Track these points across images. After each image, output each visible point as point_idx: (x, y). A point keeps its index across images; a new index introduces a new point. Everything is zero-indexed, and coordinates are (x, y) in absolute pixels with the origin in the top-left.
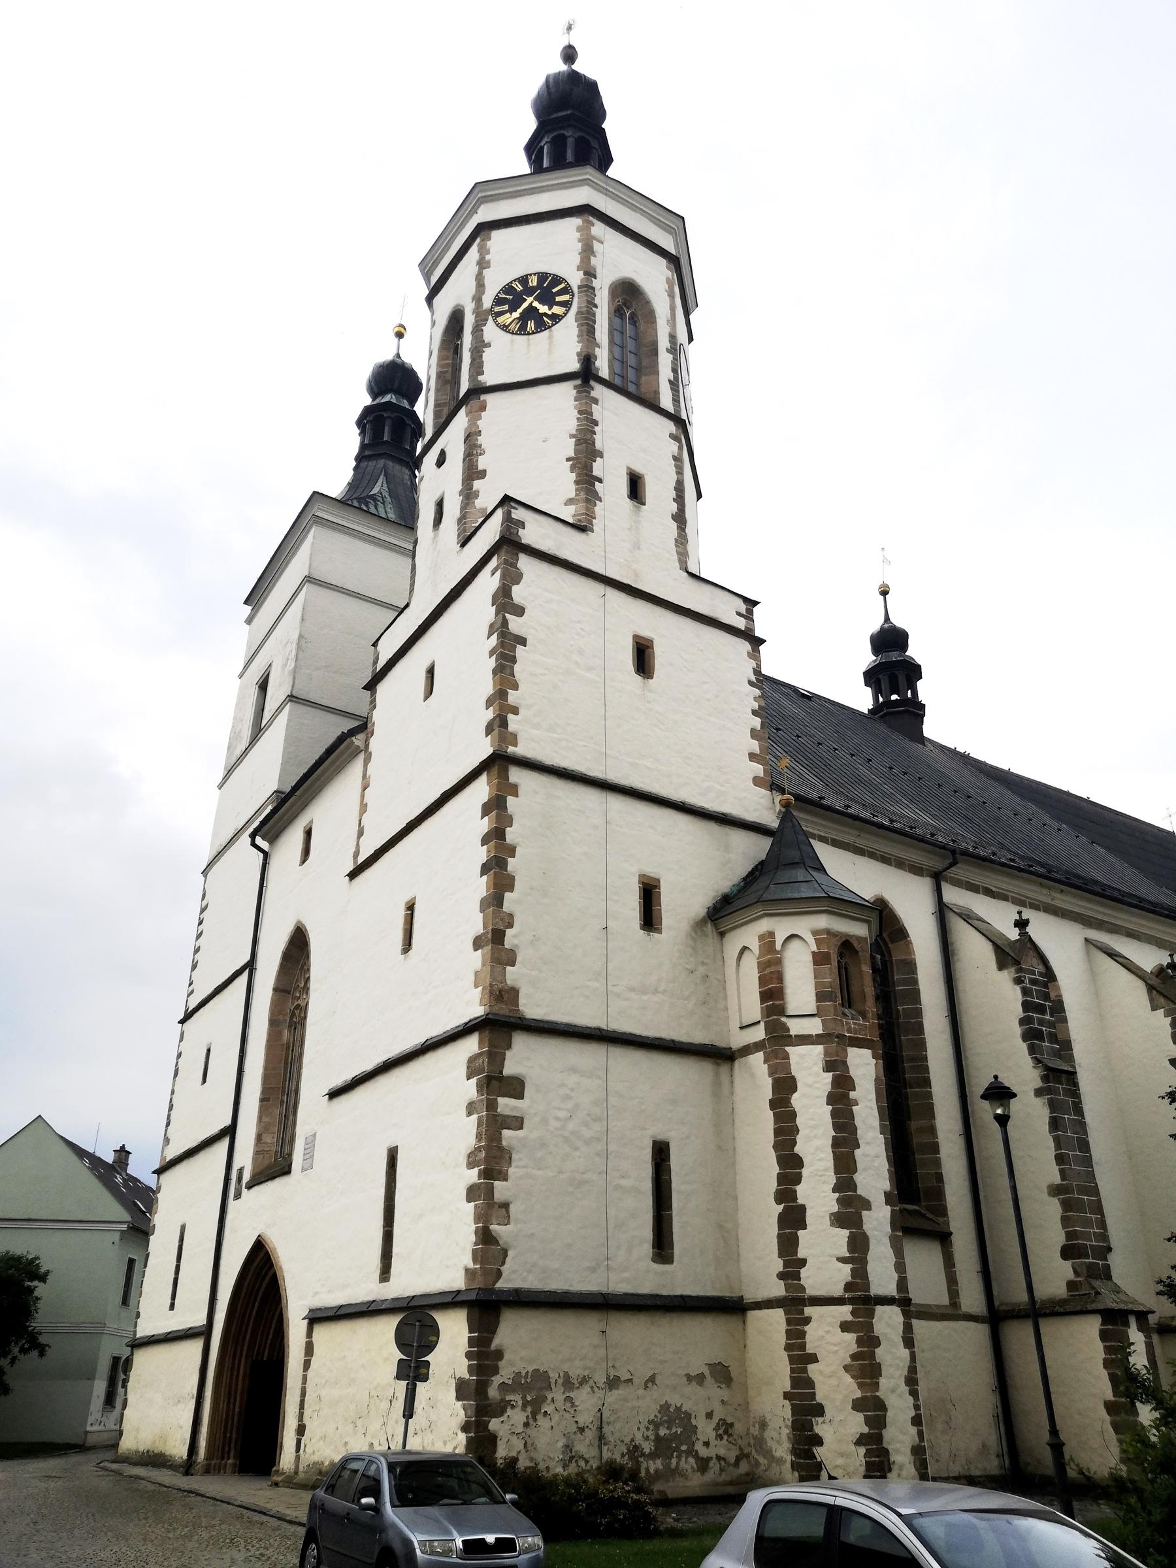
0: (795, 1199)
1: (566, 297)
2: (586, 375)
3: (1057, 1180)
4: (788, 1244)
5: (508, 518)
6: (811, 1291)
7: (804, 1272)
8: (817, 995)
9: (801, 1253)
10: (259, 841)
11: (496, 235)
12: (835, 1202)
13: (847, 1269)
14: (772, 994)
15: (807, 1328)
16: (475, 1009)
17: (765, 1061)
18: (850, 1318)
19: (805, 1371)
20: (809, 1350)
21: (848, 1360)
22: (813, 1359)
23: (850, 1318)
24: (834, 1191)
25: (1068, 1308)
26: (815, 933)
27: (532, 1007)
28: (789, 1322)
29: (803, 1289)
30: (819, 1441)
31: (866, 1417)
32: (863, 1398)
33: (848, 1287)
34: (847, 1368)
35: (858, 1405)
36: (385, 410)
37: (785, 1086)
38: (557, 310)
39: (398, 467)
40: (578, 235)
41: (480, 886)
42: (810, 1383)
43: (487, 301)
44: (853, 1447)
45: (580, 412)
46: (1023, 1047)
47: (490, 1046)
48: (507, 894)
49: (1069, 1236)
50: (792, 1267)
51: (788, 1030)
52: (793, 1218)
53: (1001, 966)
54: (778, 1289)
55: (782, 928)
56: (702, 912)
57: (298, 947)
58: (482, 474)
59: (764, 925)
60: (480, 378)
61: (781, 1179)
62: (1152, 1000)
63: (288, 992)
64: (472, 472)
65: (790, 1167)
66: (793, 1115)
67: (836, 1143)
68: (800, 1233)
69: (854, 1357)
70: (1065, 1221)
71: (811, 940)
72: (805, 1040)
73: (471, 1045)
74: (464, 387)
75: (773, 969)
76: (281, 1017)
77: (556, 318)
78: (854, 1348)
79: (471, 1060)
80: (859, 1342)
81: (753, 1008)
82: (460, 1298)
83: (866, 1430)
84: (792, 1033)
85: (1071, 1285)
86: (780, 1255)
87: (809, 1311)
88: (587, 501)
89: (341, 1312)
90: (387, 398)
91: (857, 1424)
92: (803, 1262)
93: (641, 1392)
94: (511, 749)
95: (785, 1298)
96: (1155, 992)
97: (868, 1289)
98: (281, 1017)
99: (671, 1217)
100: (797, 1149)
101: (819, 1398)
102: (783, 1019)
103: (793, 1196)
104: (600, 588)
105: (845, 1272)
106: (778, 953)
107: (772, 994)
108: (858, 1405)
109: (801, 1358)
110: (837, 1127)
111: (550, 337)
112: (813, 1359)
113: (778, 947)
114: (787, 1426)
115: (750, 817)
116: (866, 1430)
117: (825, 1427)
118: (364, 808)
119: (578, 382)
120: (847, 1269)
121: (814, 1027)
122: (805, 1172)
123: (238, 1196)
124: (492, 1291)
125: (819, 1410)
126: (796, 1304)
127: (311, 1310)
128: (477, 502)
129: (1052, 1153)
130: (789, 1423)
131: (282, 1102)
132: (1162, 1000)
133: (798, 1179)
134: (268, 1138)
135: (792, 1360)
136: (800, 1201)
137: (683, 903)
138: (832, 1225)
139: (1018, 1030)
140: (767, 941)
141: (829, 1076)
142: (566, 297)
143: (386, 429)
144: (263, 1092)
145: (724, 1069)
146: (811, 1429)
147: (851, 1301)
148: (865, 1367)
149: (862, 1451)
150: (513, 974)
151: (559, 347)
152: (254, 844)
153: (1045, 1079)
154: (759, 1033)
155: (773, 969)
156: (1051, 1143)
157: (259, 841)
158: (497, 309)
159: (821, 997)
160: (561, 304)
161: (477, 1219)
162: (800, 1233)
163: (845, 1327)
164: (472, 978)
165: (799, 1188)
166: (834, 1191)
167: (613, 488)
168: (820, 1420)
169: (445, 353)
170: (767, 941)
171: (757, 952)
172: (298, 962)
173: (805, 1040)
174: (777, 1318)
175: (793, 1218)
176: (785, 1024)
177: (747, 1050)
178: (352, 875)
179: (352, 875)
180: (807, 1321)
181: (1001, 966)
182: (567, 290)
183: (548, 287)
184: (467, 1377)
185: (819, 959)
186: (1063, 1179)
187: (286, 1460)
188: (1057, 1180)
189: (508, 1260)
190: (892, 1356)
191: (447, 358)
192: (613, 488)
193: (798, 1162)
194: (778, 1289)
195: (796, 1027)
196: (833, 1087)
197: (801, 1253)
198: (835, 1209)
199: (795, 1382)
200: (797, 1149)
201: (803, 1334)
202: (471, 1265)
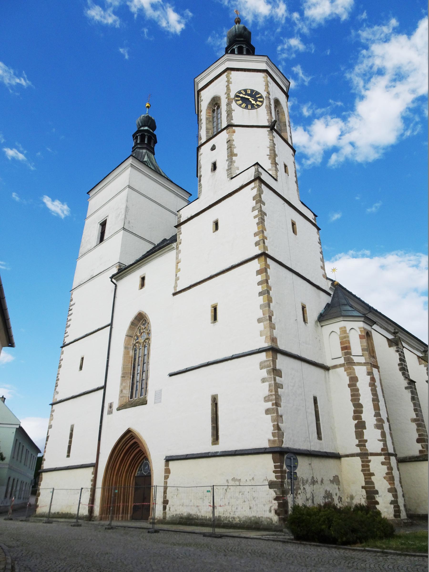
0: (361, 419)
1: (262, 100)
2: (272, 127)
3: (415, 417)
4: (359, 435)
5: (257, 171)
6: (370, 451)
7: (367, 444)
8: (362, 349)
9: (365, 438)
10: (113, 280)
11: (233, 72)
12: (375, 420)
13: (382, 443)
14: (346, 348)
15: (370, 464)
16: (265, 345)
17: (345, 371)
18: (384, 460)
19: (370, 479)
20: (371, 471)
21: (385, 475)
22: (373, 474)
23: (384, 460)
24: (374, 416)
25: (421, 459)
26: (360, 328)
27: (281, 346)
28: (362, 462)
29: (367, 450)
30: (377, 503)
31: (393, 495)
32: (391, 488)
33: (382, 450)
34: (384, 478)
35: (390, 491)
36: (146, 132)
37: (353, 380)
38: (258, 103)
39: (150, 153)
40: (263, 79)
41: (261, 300)
42: (372, 483)
43: (232, 95)
44: (389, 505)
45: (270, 140)
46: (400, 373)
47: (273, 357)
48: (271, 304)
49: (420, 435)
50: (362, 443)
51: (353, 360)
52: (360, 426)
53: (390, 346)
54: (358, 450)
55: (349, 325)
56: (317, 319)
57: (141, 319)
58: (236, 155)
59: (342, 324)
60: (232, 121)
61: (355, 412)
62: (419, 362)
63: (132, 337)
64: (231, 154)
65: (358, 409)
66: (358, 390)
67: (373, 400)
68: (364, 431)
69: (387, 474)
70: (418, 430)
71: (358, 330)
72: (359, 364)
73: (263, 356)
74: (224, 125)
75: (346, 339)
76: (129, 346)
77: (259, 106)
78: (386, 471)
79: (261, 363)
80: (388, 468)
81: (339, 352)
82: (267, 450)
83: (393, 499)
84: (355, 361)
85: (420, 451)
86: (357, 438)
87: (370, 458)
88: (276, 170)
89: (188, 457)
90: (146, 128)
91: (390, 497)
92: (366, 441)
93: (320, 486)
94: (267, 252)
95: (361, 453)
96: (420, 359)
97: (388, 451)
98: (129, 346)
99: (320, 423)
100: (360, 402)
101: (376, 488)
102: (352, 357)
103: (360, 418)
104: (283, 202)
105: (381, 445)
106: (348, 334)
107: (346, 348)
108: (390, 491)
109: (368, 474)
110: (373, 394)
111: (257, 112)
112: (373, 474)
113: (348, 332)
114: (364, 498)
115: (324, 288)
116: (393, 499)
117: (379, 498)
118: (178, 270)
119: (269, 129)
120: (382, 443)
121: (362, 360)
122: (364, 409)
123: (110, 412)
124: (281, 448)
125: (377, 492)
126: (364, 456)
127: (166, 457)
128: (235, 164)
129: (412, 408)
130: (365, 497)
131: (130, 378)
132: (423, 362)
133: (361, 412)
134: (124, 391)
135: (365, 475)
136: (363, 420)
137: (313, 314)
138: (375, 428)
139: (398, 368)
140: (343, 330)
141: (369, 377)
142: (262, 100)
143: (146, 139)
144: (123, 374)
145: (327, 372)
146: (374, 498)
147: (384, 455)
148: (390, 477)
149: (392, 506)
150: (276, 333)
151: (261, 116)
152: (112, 281)
153: (409, 384)
154: (342, 361)
155: (346, 339)
156: (412, 405)
157: (113, 280)
158: (236, 99)
159: (363, 350)
160: (260, 101)
161: (273, 421)
162: (364, 431)
163: (383, 463)
164: (259, 333)
165: (362, 415)
166: (374, 416)
167: (281, 167)
168: (377, 496)
169: (209, 111)
170: (343, 330)
171: (339, 333)
172: (137, 326)
173: (359, 364)
174: (358, 461)
175: (360, 426)
176: (352, 358)
177: (335, 367)
178: (174, 294)
179: (174, 294)
180: (369, 461)
181: (390, 346)
182: (261, 97)
183: (254, 94)
184: (275, 480)
185: (361, 337)
186: (417, 417)
187: (158, 512)
188: (415, 417)
189: (284, 436)
190: (395, 473)
191: (210, 113)
192: (281, 167)
193: (361, 406)
194: (358, 450)
195: (356, 360)
196: (350, 382)
197: (365, 438)
198: (375, 423)
199: (366, 483)
200: (360, 402)
201: (368, 466)
202: (272, 438)
